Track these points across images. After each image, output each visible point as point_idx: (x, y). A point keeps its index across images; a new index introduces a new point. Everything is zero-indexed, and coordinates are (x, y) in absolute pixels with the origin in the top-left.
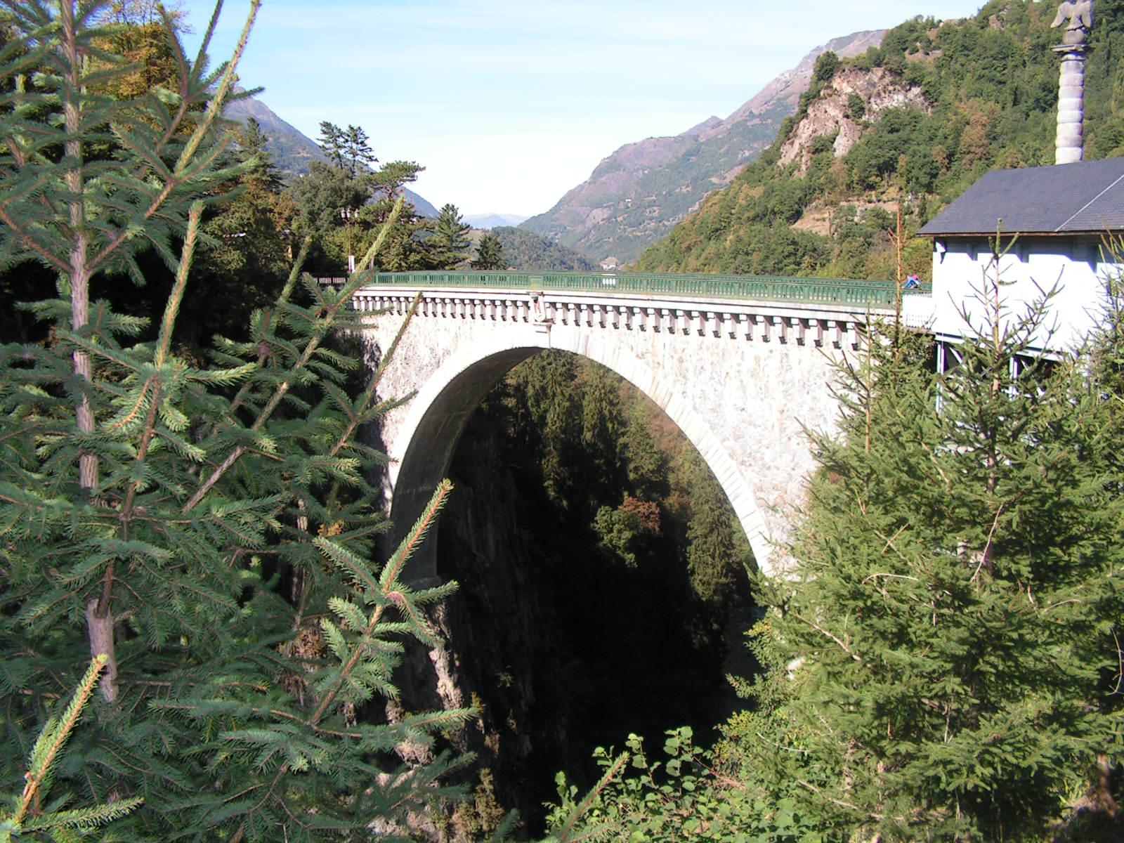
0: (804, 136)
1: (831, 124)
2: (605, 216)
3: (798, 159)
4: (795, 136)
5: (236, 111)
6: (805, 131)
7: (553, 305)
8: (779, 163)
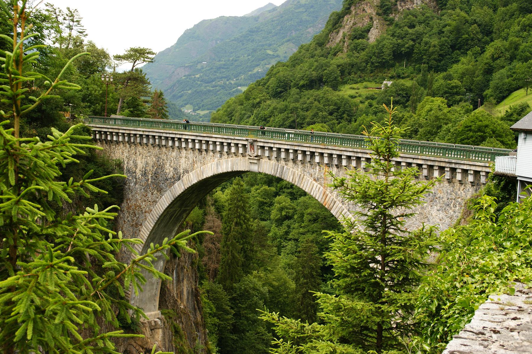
0: (347, 27)
1: (367, 21)
2: (187, 73)
3: (341, 44)
4: (341, 26)
5: (318, 85)
6: (348, 22)
7: (263, 148)
8: (328, 46)
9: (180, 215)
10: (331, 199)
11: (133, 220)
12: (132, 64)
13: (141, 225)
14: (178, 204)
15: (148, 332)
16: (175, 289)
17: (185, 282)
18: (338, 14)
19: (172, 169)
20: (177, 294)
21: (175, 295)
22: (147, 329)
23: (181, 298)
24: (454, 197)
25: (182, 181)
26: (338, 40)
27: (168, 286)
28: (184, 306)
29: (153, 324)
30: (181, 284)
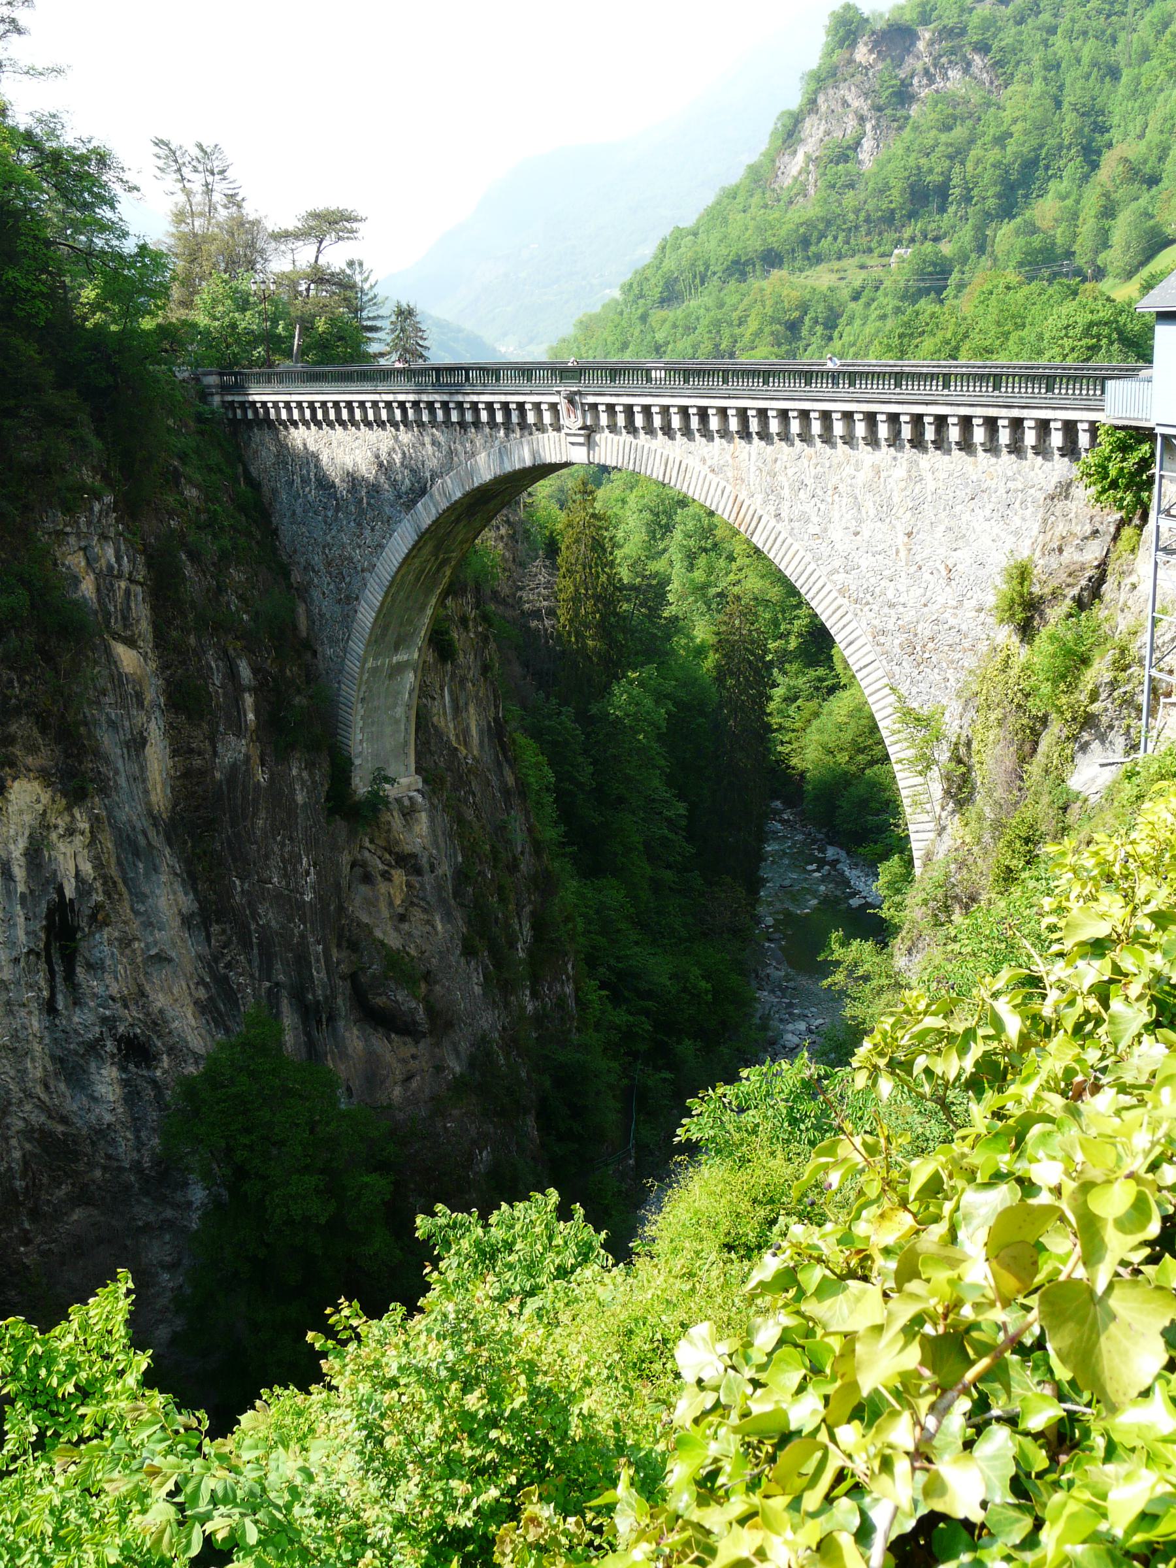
9: (438, 570)
10: (751, 512)
11: (339, 590)
12: (315, 247)
13: (357, 598)
14: (429, 548)
15: (397, 822)
16: (451, 726)
17: (472, 710)
18: (791, 114)
19: (406, 472)
20: (457, 736)
21: (453, 738)
22: (395, 814)
23: (466, 744)
24: (1020, 487)
25: (431, 496)
26: (794, 171)
27: (435, 719)
28: (474, 758)
29: (407, 802)
30: (464, 715)
